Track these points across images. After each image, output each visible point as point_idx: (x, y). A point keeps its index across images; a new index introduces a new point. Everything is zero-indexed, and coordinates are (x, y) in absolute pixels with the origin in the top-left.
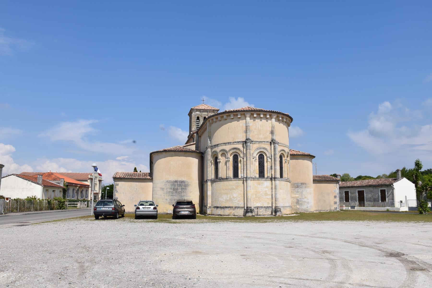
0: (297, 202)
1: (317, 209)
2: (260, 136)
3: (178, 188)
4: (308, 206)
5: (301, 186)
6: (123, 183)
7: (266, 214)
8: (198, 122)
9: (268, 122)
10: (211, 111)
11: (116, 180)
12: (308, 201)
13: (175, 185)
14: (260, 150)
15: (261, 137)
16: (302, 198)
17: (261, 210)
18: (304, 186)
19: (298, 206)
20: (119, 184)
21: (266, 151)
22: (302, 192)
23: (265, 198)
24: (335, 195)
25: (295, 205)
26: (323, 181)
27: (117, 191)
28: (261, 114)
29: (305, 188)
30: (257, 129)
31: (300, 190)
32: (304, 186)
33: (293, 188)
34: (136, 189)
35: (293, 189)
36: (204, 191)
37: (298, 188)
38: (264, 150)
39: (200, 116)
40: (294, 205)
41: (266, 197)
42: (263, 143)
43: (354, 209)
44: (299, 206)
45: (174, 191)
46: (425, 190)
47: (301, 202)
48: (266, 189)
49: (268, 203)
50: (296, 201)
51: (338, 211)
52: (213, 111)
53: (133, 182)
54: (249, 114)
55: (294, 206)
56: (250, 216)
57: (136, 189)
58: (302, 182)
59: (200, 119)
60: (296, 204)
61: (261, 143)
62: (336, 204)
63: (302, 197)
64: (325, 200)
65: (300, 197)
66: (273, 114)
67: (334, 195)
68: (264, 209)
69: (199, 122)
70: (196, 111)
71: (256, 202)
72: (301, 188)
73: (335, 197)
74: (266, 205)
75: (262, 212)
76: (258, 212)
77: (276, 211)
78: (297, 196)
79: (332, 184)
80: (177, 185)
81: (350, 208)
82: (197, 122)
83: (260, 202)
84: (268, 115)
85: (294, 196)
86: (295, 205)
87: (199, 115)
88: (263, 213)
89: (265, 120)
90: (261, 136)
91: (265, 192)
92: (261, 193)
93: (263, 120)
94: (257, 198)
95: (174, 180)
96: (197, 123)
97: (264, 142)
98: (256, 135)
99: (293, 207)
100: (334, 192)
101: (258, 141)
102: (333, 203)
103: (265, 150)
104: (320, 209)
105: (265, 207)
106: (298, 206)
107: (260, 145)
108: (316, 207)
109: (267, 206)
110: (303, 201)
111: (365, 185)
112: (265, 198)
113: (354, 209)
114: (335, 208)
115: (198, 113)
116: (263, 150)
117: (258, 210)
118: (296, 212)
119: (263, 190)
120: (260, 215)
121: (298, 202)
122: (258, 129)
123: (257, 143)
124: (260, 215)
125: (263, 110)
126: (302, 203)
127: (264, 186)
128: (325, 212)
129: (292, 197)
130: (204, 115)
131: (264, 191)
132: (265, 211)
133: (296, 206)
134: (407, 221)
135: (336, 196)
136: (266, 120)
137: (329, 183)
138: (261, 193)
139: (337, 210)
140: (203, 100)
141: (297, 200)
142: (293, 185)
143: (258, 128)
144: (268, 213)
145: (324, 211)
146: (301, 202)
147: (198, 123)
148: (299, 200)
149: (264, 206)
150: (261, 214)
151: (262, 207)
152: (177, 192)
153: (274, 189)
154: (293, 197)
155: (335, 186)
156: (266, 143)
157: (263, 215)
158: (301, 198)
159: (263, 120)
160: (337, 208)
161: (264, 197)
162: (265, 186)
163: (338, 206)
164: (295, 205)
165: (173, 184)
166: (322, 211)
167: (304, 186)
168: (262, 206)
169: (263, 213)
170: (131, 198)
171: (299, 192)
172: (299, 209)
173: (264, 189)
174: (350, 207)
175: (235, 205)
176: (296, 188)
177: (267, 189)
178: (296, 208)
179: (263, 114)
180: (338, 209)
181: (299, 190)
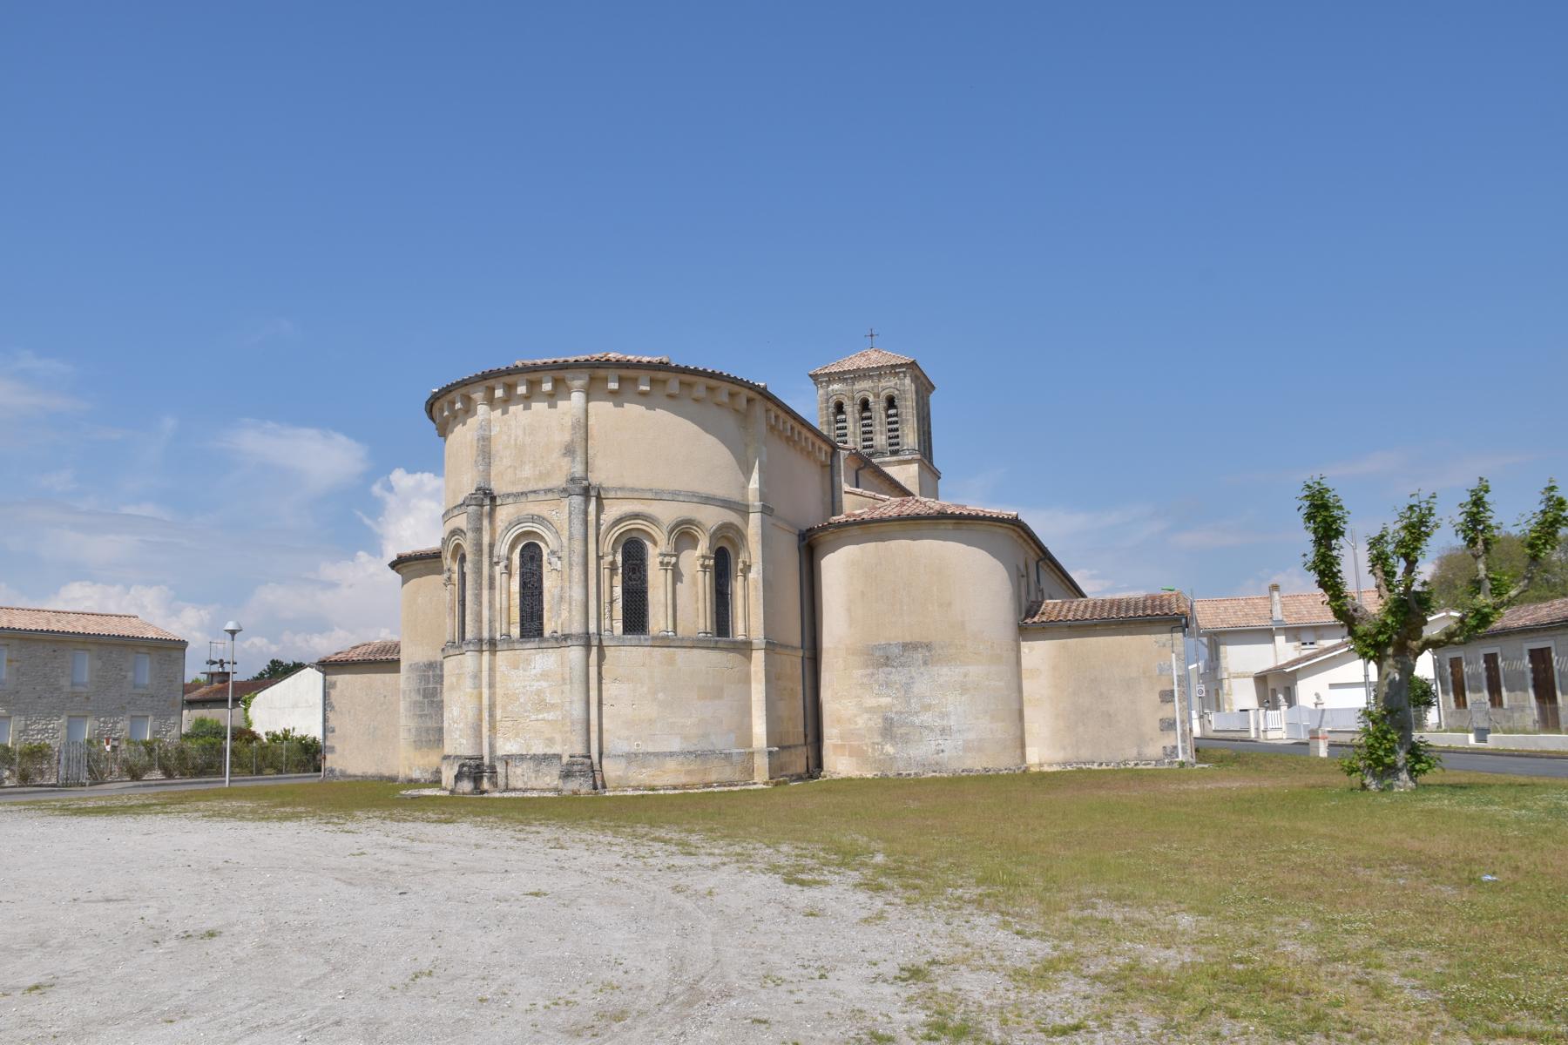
0: (886, 729)
1: (1060, 756)
2: (521, 471)
3: (436, 688)
4: (941, 747)
5: (902, 656)
6: (347, 677)
7: (540, 784)
8: (840, 422)
9: (623, 406)
10: (885, 373)
11: (329, 671)
12: (945, 722)
13: (429, 677)
14: (519, 526)
15: (527, 477)
16: (907, 712)
17: (519, 771)
18: (920, 655)
19: (889, 749)
20: (338, 683)
21: (541, 527)
22: (907, 687)
23: (537, 720)
24: (1168, 688)
25: (878, 744)
26: (1096, 625)
27: (333, 707)
28: (544, 380)
29: (925, 663)
30: (513, 442)
31: (898, 676)
32: (920, 655)
33: (867, 666)
34: (385, 697)
35: (869, 671)
36: (807, 683)
37: (887, 665)
38: (534, 525)
39: (846, 398)
40: (873, 743)
41: (540, 717)
42: (531, 497)
43: (1485, 741)
44: (892, 745)
45: (426, 700)
46: (1390, 651)
47: (902, 731)
48: (539, 683)
49: (547, 739)
50: (881, 726)
51: (1182, 764)
52: (890, 372)
53: (377, 673)
54: (480, 389)
55: (873, 749)
56: (465, 791)
57: (385, 697)
58: (908, 640)
59: (871, 405)
60: (879, 740)
61: (523, 499)
62: (1172, 733)
63: (908, 703)
64: (1110, 716)
65: (899, 708)
66: (567, 374)
67: (1159, 689)
68: (532, 764)
69: (896, 415)
70: (829, 382)
71: (504, 738)
72: (902, 665)
73: (1168, 698)
74: (539, 749)
75: (523, 775)
76: (509, 777)
77: (587, 767)
78: (885, 701)
79: (1150, 634)
80: (434, 676)
81: (1472, 738)
82: (837, 422)
83: (517, 735)
84: (548, 382)
85: (871, 702)
86: (876, 741)
87: (842, 396)
88: (526, 779)
89: (545, 402)
90: (527, 471)
91: (536, 697)
92: (522, 700)
93: (533, 404)
94: (507, 719)
95: (425, 660)
96: (840, 425)
97: (533, 495)
98: (509, 470)
99: (870, 750)
100: (1161, 674)
101: (514, 491)
102: (1157, 725)
103: (538, 526)
104: (1085, 754)
105: (534, 757)
106: (889, 749)
107: (521, 506)
108: (1064, 748)
109: (545, 755)
110: (913, 725)
111: (1547, 620)
112: (537, 720)
113: (1485, 741)
114: (1168, 751)
115: (836, 387)
116: (531, 524)
117: (509, 768)
118: (1230, 768)
119: (528, 688)
120: (515, 790)
121: (889, 729)
122: (516, 444)
123: (510, 500)
124: (515, 790)
125: (520, 364)
126: (907, 734)
127: (533, 672)
128: (1110, 767)
129: (866, 708)
130: (861, 393)
131: (532, 692)
132: (533, 775)
133: (883, 749)
134: (662, 833)
135: (1172, 692)
136: (546, 404)
137: (1130, 633)
138: (522, 700)
139: (1177, 757)
140: (872, 336)
141: (886, 719)
142: (866, 657)
143: (516, 440)
144: (549, 781)
145: (1104, 767)
146: (902, 731)
147: (869, 421)
148: (892, 719)
149: (532, 752)
150: (520, 785)
151: (522, 757)
152: (433, 702)
153: (592, 685)
154: (867, 705)
155: (1164, 646)
156: (542, 497)
157: (525, 790)
158: (901, 713)
159: (533, 404)
160: (1175, 747)
161: (533, 717)
162: (538, 671)
163: (1184, 741)
164: (878, 744)
165: (424, 675)
166: (1095, 767)
167: (919, 656)
168: (525, 753)
169: (525, 783)
170: (371, 726)
171: (895, 683)
172: (892, 759)
173: (532, 683)
174: (1471, 732)
175: (638, 745)
176: (880, 670)
177: (544, 684)
178: (881, 757)
179: (525, 381)
180: (1184, 752)
181: (895, 677)
